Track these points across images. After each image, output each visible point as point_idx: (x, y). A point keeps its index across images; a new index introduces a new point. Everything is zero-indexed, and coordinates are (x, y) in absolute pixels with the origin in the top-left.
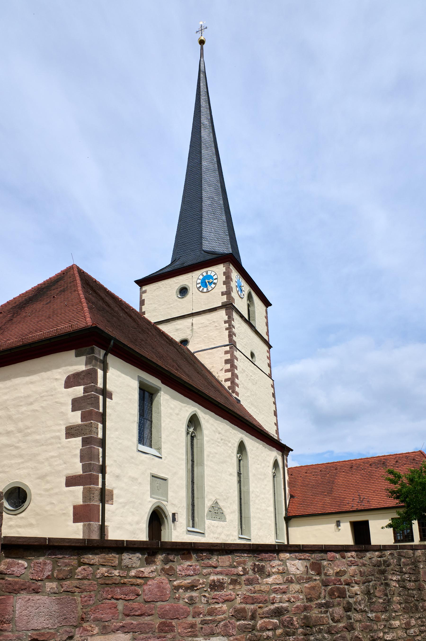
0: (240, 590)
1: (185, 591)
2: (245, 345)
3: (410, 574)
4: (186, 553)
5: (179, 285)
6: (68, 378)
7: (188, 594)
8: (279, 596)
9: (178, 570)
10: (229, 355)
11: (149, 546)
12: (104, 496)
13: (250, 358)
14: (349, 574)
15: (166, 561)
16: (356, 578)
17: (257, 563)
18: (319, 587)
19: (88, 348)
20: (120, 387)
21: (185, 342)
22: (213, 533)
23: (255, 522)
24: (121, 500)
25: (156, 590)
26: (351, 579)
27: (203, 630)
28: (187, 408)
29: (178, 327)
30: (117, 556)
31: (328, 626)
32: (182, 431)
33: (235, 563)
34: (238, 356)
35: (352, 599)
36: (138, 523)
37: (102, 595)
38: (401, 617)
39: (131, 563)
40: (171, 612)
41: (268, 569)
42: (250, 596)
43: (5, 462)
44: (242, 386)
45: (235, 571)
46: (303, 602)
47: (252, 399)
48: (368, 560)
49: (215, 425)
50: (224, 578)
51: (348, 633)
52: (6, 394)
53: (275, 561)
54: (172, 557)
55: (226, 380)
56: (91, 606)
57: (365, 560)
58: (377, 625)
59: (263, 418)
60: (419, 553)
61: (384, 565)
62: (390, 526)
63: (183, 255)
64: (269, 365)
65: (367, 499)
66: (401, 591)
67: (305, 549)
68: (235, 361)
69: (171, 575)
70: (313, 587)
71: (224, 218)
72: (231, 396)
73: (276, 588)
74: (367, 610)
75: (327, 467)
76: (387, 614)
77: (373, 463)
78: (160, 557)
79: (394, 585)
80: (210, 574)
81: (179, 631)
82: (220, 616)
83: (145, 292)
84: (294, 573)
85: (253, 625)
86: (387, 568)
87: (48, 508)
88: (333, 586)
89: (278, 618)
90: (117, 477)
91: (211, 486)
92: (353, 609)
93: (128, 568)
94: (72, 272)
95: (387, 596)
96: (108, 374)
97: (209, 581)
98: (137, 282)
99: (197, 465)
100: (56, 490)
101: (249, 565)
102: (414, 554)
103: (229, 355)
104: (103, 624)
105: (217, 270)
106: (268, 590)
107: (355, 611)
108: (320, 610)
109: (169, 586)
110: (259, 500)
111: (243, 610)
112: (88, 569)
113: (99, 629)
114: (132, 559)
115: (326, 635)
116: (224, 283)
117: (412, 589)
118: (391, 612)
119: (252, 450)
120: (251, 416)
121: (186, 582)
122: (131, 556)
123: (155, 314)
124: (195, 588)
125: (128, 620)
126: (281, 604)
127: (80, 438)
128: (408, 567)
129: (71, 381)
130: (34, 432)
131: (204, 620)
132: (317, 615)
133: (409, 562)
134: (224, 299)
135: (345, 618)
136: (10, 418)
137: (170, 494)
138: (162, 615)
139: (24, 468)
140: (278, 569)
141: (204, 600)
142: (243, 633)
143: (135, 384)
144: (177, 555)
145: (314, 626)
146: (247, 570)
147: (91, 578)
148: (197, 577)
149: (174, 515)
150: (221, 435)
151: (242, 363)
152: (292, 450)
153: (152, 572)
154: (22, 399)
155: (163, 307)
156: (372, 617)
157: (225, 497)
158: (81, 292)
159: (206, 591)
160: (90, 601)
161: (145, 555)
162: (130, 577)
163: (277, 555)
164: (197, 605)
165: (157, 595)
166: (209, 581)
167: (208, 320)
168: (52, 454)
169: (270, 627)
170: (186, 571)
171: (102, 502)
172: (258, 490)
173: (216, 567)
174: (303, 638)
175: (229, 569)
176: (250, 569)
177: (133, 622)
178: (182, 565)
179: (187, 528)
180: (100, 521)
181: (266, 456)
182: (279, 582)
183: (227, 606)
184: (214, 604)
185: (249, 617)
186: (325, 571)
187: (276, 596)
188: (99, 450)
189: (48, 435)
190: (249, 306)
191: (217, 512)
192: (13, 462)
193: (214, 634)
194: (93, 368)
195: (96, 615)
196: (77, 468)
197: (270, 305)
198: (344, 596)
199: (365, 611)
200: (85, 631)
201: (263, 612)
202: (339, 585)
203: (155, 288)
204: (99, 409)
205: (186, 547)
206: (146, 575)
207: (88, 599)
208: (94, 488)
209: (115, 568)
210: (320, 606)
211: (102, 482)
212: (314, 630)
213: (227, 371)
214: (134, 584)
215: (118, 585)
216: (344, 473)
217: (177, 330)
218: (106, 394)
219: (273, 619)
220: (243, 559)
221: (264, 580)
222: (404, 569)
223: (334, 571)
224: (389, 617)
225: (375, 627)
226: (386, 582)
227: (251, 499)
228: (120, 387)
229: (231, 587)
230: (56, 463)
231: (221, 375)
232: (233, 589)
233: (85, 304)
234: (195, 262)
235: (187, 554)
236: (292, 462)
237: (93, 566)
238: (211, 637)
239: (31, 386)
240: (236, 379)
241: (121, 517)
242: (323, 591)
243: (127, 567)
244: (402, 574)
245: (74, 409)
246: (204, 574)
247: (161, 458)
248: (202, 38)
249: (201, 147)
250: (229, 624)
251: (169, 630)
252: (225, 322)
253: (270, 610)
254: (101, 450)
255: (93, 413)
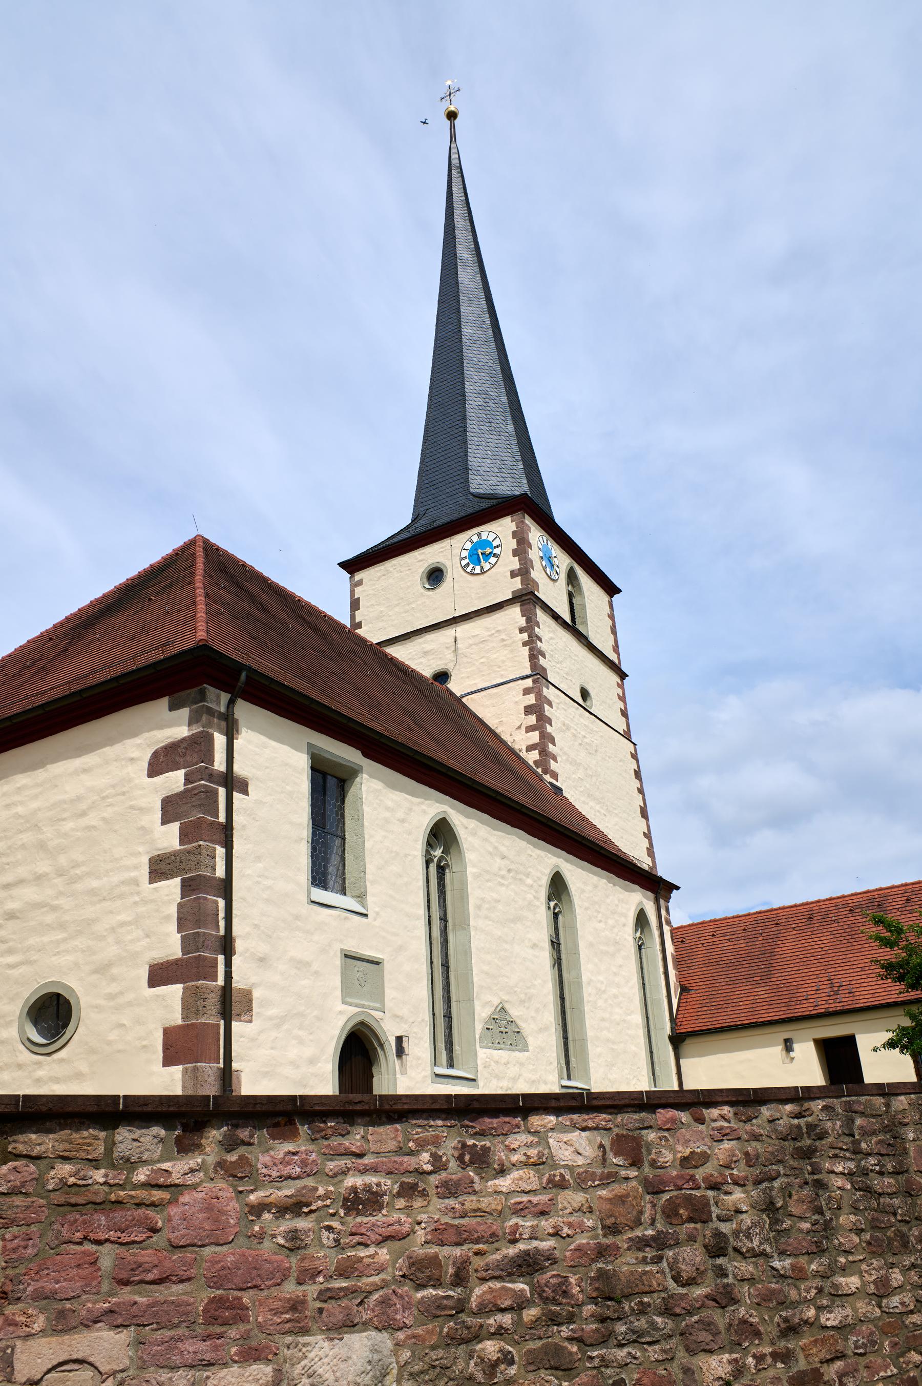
0: (424, 1209)
1: (277, 1218)
2: (567, 674)
3: (882, 1155)
4: (283, 1122)
5: (426, 565)
6: (156, 754)
7: (286, 1225)
8: (528, 1224)
9: (260, 1166)
10: (533, 695)
11: (183, 1109)
12: (231, 1004)
13: (580, 701)
14: (716, 1162)
15: (230, 1144)
16: (735, 1172)
17: (470, 1142)
18: (635, 1197)
19: (193, 692)
20: (267, 768)
21: (442, 677)
22: (498, 1077)
23: (599, 1050)
24: (272, 1012)
25: (201, 1216)
26: (721, 1174)
27: (324, 1315)
28: (424, 807)
29: (428, 647)
30: (103, 1134)
31: (663, 1295)
32: (415, 857)
33: (411, 1144)
34: (551, 698)
35: (728, 1224)
36: (312, 1061)
37: (59, 1232)
38: (864, 1267)
39: (138, 1150)
40: (240, 1272)
41: (499, 1154)
42: (452, 1226)
43: (32, 941)
44: (564, 758)
45: (410, 1162)
46: (596, 1237)
47: (590, 783)
48: (766, 1124)
49: (493, 839)
50: (382, 1181)
51: (719, 1311)
52: (36, 797)
53: (518, 1136)
54: (247, 1133)
55: (530, 748)
56: (30, 1260)
57: (760, 1125)
58: (798, 1289)
59: (616, 825)
60: (901, 1103)
61: (809, 1137)
62: (891, 1044)
63: (433, 505)
64: (624, 713)
65: (848, 987)
66: (857, 1201)
67: (595, 1103)
68: (546, 707)
69: (242, 1178)
70: (621, 1197)
71: (511, 428)
72: (542, 780)
73: (520, 1203)
74: (768, 1250)
75: (757, 922)
76: (825, 1260)
77: (858, 907)
78: (215, 1134)
79: (840, 1184)
80: (345, 1172)
81: (260, 1319)
82: (371, 1279)
83: (360, 583)
84: (570, 1163)
85: (459, 1299)
86: (818, 1143)
87: (112, 1036)
88: (675, 1193)
89: (528, 1279)
90: (262, 960)
91: (487, 973)
92: (730, 1249)
93: (131, 1164)
94: (192, 551)
95: (821, 1213)
96: (237, 743)
97: (343, 1191)
98: (345, 565)
99: (454, 929)
100: (130, 996)
101: (449, 1147)
102: (888, 1105)
103: (533, 695)
104: (59, 1306)
105: (500, 529)
106: (499, 1208)
107: (737, 1255)
108: (641, 1255)
109: (237, 1205)
110: (606, 1001)
111: (434, 1261)
112: (26, 1168)
113: (47, 1318)
114: (142, 1141)
115: (659, 1320)
116: (515, 553)
117: (889, 1194)
118: (835, 1253)
119: (583, 891)
120: (584, 819)
121: (280, 1194)
122: (138, 1133)
123: (381, 624)
124: (306, 1210)
125: (126, 1295)
126: (535, 1243)
127: (177, 881)
128: (874, 1139)
129: (160, 763)
130: (88, 874)
131: (329, 1289)
132: (632, 1268)
133: (877, 1127)
134: (517, 584)
135: (710, 1274)
136: (42, 846)
137: (390, 993)
138: (215, 1279)
139: (67, 951)
140: (525, 1154)
141: (327, 1238)
142: (431, 1321)
143: (301, 762)
144: (261, 1128)
145: (627, 1297)
146: (444, 1159)
147: (31, 1190)
148: (310, 1182)
149: (399, 1040)
150: (508, 862)
151: (562, 713)
152: (678, 888)
153: (192, 1171)
154: (65, 806)
155: (397, 609)
156: (783, 1267)
157: (522, 996)
158: (199, 585)
159: (333, 1215)
160: (25, 1247)
161: (175, 1130)
162: (135, 1187)
163: (523, 1120)
164: (309, 1251)
165: (203, 1228)
166: (343, 1191)
167: (487, 629)
168: (123, 917)
169: (507, 1303)
170: (281, 1167)
171: (224, 1019)
172: (601, 978)
173: (360, 1156)
174: (597, 1330)
175: (396, 1159)
176: (450, 1157)
177: (139, 1299)
178: (272, 1153)
179: (432, 1070)
180: (222, 1061)
181: (616, 902)
182: (528, 1188)
183: (389, 1252)
184: (353, 1247)
185: (448, 1279)
186: (653, 1156)
187: (521, 1223)
188: (217, 902)
189: (115, 879)
190: (570, 596)
191: (505, 1031)
192: (46, 939)
193: (354, 1326)
194: (203, 732)
195: (39, 1284)
196: (171, 946)
197: (618, 591)
198: (704, 1217)
199: (763, 1254)
200: (10, 1325)
201: (487, 1265)
202: (691, 1189)
203: (379, 574)
204: (216, 815)
205: (280, 1108)
206: (176, 1178)
207: (22, 1243)
208: (207, 988)
209: (95, 1163)
210: (642, 1244)
211: (226, 971)
212: (627, 1308)
213: (529, 729)
214: (144, 1204)
215: (102, 1206)
216: (795, 932)
217: (426, 653)
218: (233, 783)
219: (514, 1282)
220: (431, 1133)
221: (490, 1183)
222: (863, 1145)
223: (674, 1155)
224: (829, 1267)
225: (794, 1294)
226: (816, 1177)
227: (586, 997)
228: (267, 768)
229: (401, 1203)
230: (129, 937)
231: (517, 735)
232: (407, 1207)
233: (201, 607)
234: (455, 516)
235: (285, 1125)
236: (681, 911)
237: (38, 1162)
238: (347, 1333)
239: (84, 777)
240: (550, 746)
241: (272, 1048)
242: (649, 1206)
243: (128, 1160)
244: (859, 1156)
245: (166, 820)
246: (331, 1174)
247: (366, 915)
248: (452, 108)
249: (458, 301)
250: (394, 1298)
251: (234, 1318)
252: (522, 630)
253: (506, 1260)
254: (221, 903)
255: (204, 826)
